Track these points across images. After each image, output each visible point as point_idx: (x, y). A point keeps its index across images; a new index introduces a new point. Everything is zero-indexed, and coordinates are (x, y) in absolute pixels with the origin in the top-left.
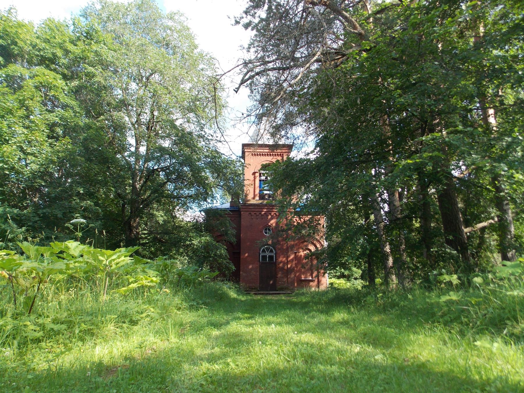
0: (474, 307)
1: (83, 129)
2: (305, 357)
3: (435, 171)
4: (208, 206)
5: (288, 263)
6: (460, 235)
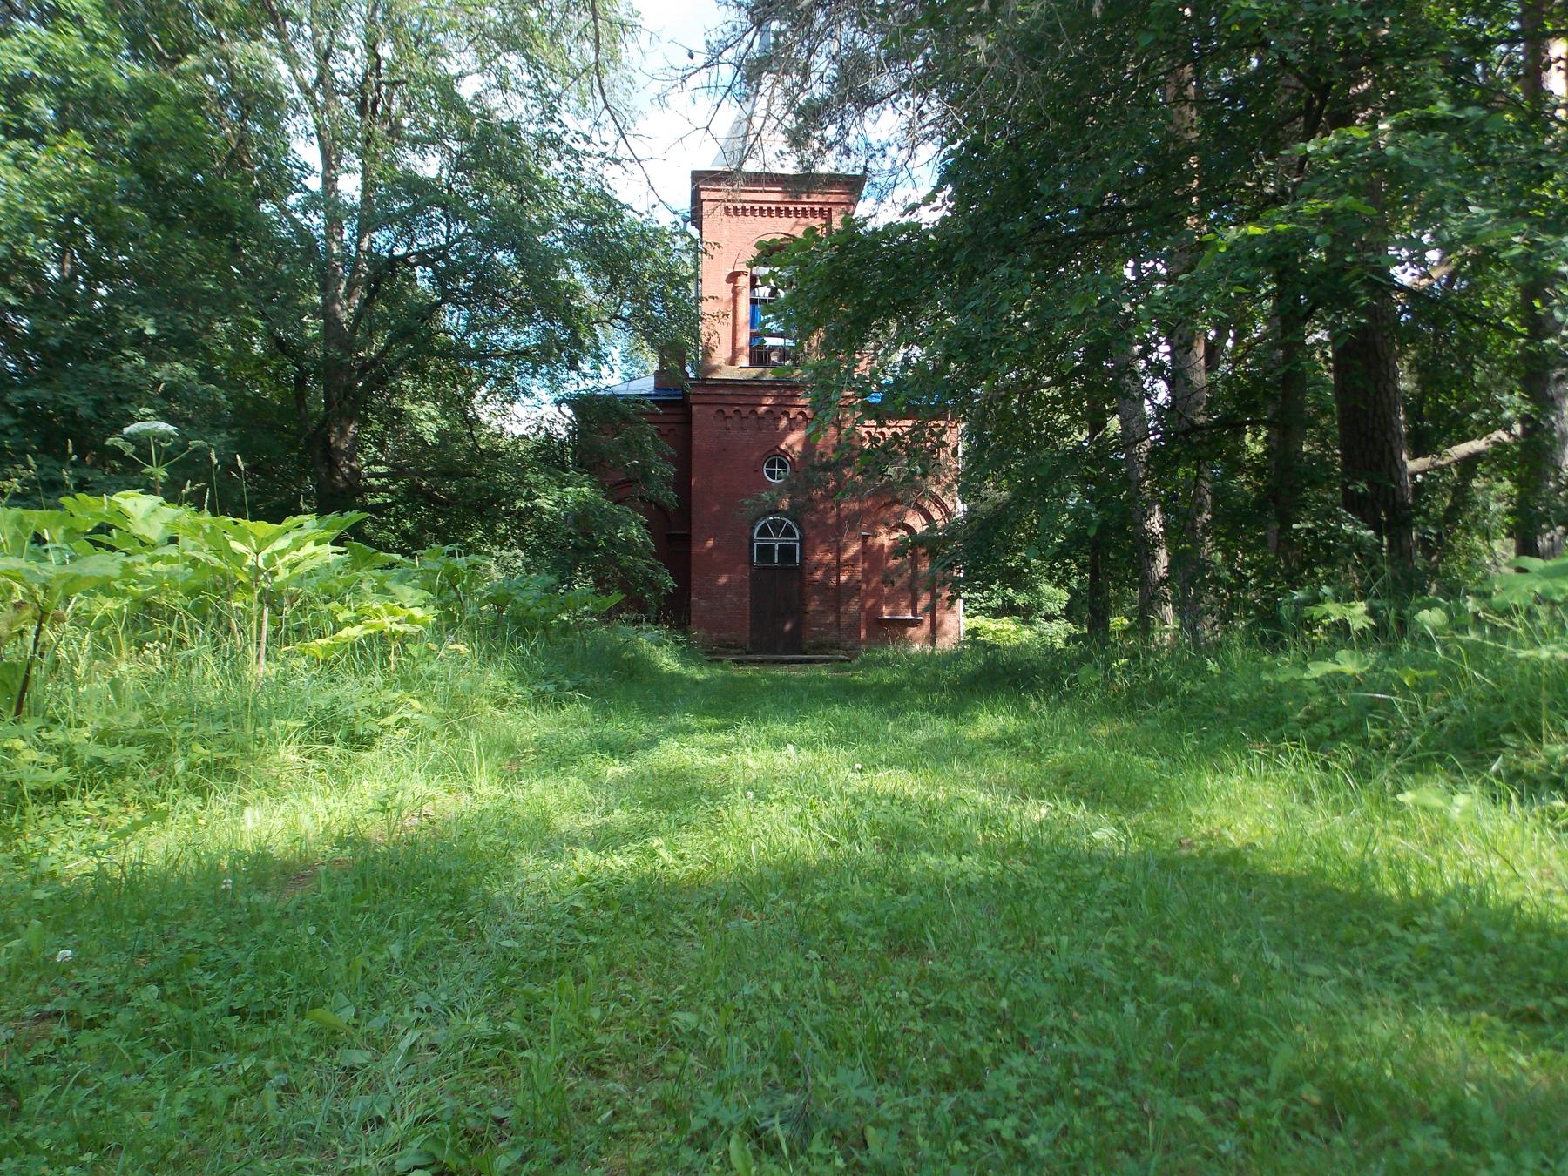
0: (1407, 696)
1: (126, 102)
2: (883, 832)
3: (1335, 265)
4: (582, 386)
5: (839, 568)
6: (1392, 479)
